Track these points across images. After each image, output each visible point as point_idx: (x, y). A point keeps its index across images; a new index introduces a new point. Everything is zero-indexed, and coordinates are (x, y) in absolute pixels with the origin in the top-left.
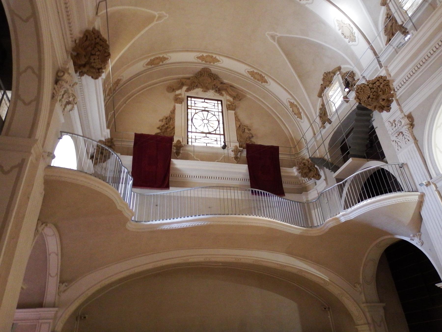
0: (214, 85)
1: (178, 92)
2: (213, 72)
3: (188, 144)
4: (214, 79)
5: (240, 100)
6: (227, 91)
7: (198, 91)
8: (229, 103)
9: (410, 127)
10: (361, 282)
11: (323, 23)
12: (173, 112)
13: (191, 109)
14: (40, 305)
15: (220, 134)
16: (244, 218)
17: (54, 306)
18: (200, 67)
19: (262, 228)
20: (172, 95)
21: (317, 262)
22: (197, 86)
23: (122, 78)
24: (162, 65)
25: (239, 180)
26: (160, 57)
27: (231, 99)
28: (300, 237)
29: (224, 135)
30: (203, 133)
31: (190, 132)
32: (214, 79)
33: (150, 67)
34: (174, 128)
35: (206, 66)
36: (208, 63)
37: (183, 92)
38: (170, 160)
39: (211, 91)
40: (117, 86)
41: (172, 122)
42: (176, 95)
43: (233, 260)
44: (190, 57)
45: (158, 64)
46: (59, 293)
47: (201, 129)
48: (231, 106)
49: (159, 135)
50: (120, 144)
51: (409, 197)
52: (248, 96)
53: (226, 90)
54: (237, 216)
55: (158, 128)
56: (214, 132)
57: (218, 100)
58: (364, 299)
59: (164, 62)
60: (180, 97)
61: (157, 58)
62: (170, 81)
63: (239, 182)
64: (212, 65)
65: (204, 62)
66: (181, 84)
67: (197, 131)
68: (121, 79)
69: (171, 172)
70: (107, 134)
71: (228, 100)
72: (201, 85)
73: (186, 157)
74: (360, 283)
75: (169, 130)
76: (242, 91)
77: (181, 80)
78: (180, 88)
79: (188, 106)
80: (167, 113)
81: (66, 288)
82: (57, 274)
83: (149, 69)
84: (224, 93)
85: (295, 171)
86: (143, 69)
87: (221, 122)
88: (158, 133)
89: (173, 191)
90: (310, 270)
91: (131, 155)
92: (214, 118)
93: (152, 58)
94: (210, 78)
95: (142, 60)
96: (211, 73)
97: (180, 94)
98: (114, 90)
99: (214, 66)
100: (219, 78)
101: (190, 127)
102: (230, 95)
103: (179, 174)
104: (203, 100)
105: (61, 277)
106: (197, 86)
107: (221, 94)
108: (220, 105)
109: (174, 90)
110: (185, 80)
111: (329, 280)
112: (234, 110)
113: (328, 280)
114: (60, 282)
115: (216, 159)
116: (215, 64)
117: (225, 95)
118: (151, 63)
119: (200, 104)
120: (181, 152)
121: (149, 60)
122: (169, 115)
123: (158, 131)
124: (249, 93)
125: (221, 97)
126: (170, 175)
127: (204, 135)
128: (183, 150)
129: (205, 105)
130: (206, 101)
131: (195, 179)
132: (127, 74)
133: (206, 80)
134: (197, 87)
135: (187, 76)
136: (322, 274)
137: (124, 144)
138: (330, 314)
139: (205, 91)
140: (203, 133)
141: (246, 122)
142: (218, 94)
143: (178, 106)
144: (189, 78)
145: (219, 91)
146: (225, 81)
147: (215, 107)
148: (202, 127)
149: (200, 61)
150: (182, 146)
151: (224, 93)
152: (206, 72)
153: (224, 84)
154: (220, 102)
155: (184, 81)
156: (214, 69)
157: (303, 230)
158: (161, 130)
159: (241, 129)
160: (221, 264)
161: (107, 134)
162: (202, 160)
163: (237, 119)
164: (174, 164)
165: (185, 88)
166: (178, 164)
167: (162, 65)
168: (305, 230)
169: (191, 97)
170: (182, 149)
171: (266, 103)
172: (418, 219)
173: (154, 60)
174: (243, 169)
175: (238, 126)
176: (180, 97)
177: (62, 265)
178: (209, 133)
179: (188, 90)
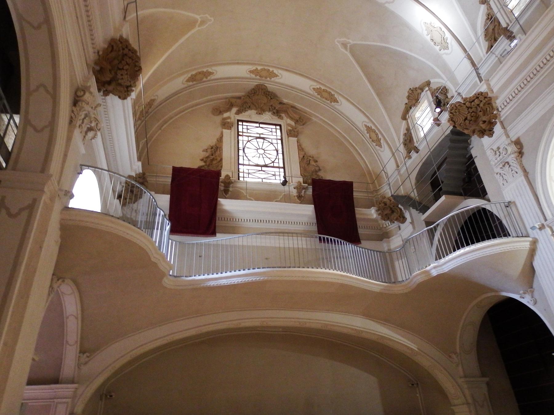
0: (272, 106)
1: (226, 115)
3: (239, 179)
4: (271, 99)
5: (304, 124)
6: (288, 114)
7: (251, 114)
8: (289, 128)
10: (458, 351)
11: (225, 211)
13: (242, 136)
14: (56, 381)
17: (73, 382)
18: (254, 83)
19: (332, 284)
20: (218, 119)
22: (250, 107)
23: (156, 98)
26: (203, 71)
27: (293, 123)
28: (380, 296)
29: (284, 168)
31: (241, 164)
32: (271, 99)
33: (191, 83)
34: (221, 160)
36: (264, 78)
37: (232, 115)
38: (217, 200)
40: (151, 107)
42: (224, 119)
43: (297, 325)
49: (203, 168)
51: (518, 244)
55: (202, 160)
56: (272, 165)
59: (209, 78)
60: (229, 120)
61: (200, 73)
64: (268, 81)
65: (258, 77)
66: (230, 105)
67: (251, 163)
69: (218, 214)
71: (289, 125)
72: (255, 106)
73: (237, 196)
76: (306, 113)
78: (229, 110)
80: (213, 142)
81: (87, 359)
84: (283, 115)
85: (373, 213)
86: (183, 86)
87: (280, 151)
88: (201, 167)
89: (220, 238)
91: (167, 194)
93: (194, 73)
94: (266, 97)
97: (229, 118)
99: (271, 82)
100: (277, 96)
102: (292, 119)
103: (229, 218)
104: (258, 125)
105: (81, 344)
107: (280, 117)
108: (278, 131)
109: (221, 113)
111: (418, 349)
113: (416, 350)
114: (80, 352)
117: (285, 118)
118: (192, 79)
119: (255, 130)
120: (231, 189)
121: (189, 75)
123: (202, 164)
126: (217, 219)
127: (260, 168)
129: (260, 131)
130: (261, 125)
132: (163, 92)
133: (261, 100)
134: (250, 108)
137: (160, 180)
139: (260, 114)
140: (257, 165)
141: (311, 151)
142: (277, 118)
143: (226, 131)
144: (239, 98)
145: (277, 113)
146: (285, 101)
147: (273, 134)
150: (232, 183)
151: (283, 115)
153: (284, 104)
155: (233, 101)
156: (271, 86)
158: (205, 162)
159: (306, 160)
160: (281, 330)
163: (300, 148)
164: (222, 205)
165: (234, 110)
168: (387, 286)
169: (242, 121)
172: (530, 272)
173: (196, 74)
174: (309, 210)
175: (302, 156)
178: (266, 166)
179: (238, 113)
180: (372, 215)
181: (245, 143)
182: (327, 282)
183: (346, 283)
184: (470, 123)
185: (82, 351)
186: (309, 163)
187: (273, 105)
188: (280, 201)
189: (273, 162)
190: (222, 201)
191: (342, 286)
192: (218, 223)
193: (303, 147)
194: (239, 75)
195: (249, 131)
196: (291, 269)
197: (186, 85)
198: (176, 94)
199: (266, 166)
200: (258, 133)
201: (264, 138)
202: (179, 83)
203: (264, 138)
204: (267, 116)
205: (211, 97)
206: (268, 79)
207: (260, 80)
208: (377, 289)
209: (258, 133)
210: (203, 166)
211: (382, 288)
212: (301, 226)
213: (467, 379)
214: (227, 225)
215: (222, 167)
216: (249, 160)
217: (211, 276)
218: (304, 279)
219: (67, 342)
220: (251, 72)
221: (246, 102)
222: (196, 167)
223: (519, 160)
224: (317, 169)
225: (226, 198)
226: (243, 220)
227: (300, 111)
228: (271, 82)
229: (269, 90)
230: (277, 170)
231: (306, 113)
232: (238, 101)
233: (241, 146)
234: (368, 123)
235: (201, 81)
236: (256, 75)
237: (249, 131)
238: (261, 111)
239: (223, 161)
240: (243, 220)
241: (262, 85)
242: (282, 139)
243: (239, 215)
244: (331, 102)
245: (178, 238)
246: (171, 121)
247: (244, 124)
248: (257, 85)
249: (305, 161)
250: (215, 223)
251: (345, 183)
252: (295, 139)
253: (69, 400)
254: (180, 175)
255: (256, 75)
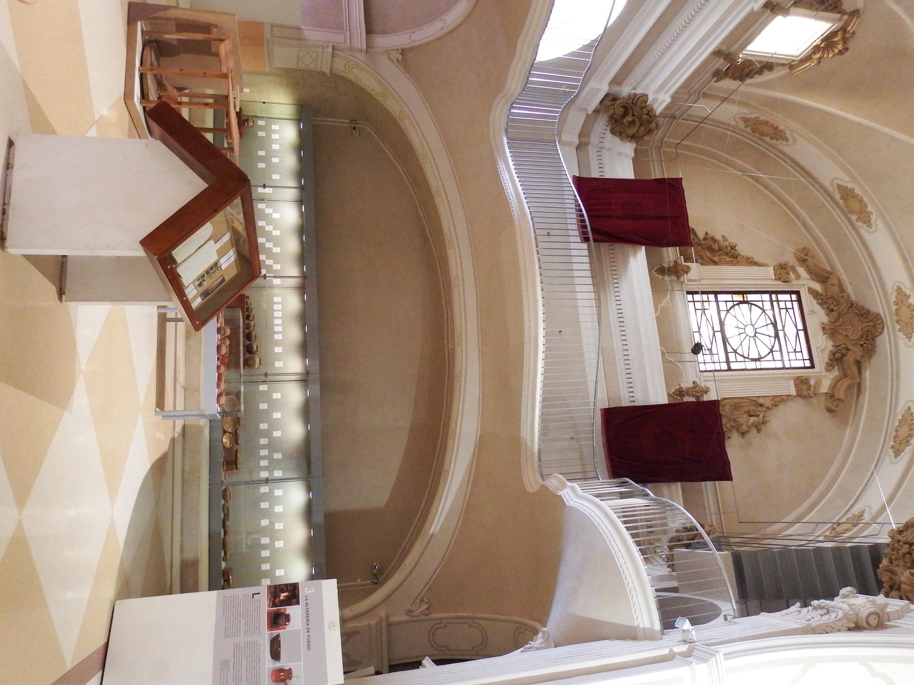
0: (848, 349)
1: (801, 271)
2: (879, 340)
3: (688, 293)
4: (862, 346)
5: (829, 410)
6: (842, 379)
7: (818, 316)
8: (812, 382)
9: (849, 620)
10: (433, 616)
11: (626, 262)
12: (751, 262)
13: (771, 301)
14: (369, 31)
15: (728, 362)
16: (536, 301)
17: (368, 46)
18: (878, 306)
19: (520, 328)
20: (791, 260)
21: (469, 509)
22: (832, 311)
23: (791, 142)
24: (851, 223)
25: (631, 394)
26: (866, 206)
27: (825, 387)
28: (515, 442)
29: (729, 369)
30: (722, 324)
31: (716, 297)
32: (862, 346)
33: (837, 196)
34: (715, 263)
35: (888, 319)
36: (895, 318)
37: (805, 282)
38: (641, 244)
39: (831, 343)
40: (772, 138)
41: (728, 259)
42: (793, 269)
43: (457, 331)
44: (894, 272)
45: (850, 212)
46: (387, 52)
47: (730, 322)
48: (805, 387)
49: (692, 236)
50: (655, 158)
51: (643, 604)
52: (848, 430)
53: (845, 375)
54: (538, 278)
55: (706, 234)
56: (729, 350)
57: (811, 359)
58: (395, 619)
59: (859, 224)
60: (792, 276)
61: (861, 201)
62: (821, 254)
63: (627, 395)
64: (893, 327)
65: (894, 307)
66: (822, 276)
67: (723, 314)
68: (787, 140)
69: (617, 246)
70: (663, 101)
71: (818, 383)
72: (837, 320)
74: (429, 614)
75: (708, 254)
76: (855, 415)
77: (831, 273)
79: (777, 293)
80: (743, 249)
81: (395, 60)
82: (414, 41)
83: (832, 198)
86: (826, 182)
87: (759, 365)
88: (695, 234)
89: (580, 251)
90: (449, 489)
92: (764, 351)
93: (857, 191)
94: (862, 336)
95: (847, 171)
96: (874, 338)
97: (798, 277)
98: (762, 134)
99: (894, 333)
100: (870, 357)
101: (728, 297)
102: (834, 386)
103: (618, 268)
104: (800, 326)
105: (411, 49)
106: (832, 311)
107: (830, 366)
108: (801, 364)
110: (836, 283)
111: (432, 535)
112: (799, 395)
113: (432, 531)
114: (403, 50)
115: (666, 348)
116: (900, 334)
118: (847, 194)
119: (791, 326)
120: (667, 278)
121: (850, 186)
122: (740, 252)
123: (701, 235)
124: (857, 429)
125: (823, 366)
126: (633, 404)
127: (717, 328)
128: (671, 281)
129: (791, 331)
130: (802, 334)
131: (596, 162)
132: (804, 149)
133: (853, 332)
135: (850, 289)
136: (444, 515)
137: (656, 165)
138: (364, 585)
139: (824, 328)
140: (722, 324)
141: (779, 420)
142: (827, 360)
143: (771, 271)
144: (842, 289)
145: (837, 359)
146: (867, 374)
148: (735, 323)
149: (893, 298)
150: (679, 278)
151: (836, 373)
152: (871, 324)
153: (860, 373)
154: (794, 297)
155: (833, 280)
156: (884, 341)
157: (532, 440)
158: (705, 239)
159: (757, 411)
160: (451, 347)
161: (663, 101)
162: (659, 320)
163: (779, 401)
164: (635, 254)
165: (817, 287)
166: (638, 261)
167: (851, 223)
168: (533, 453)
169: (799, 301)
170: (674, 278)
171: (844, 471)
172: (586, 632)
173: (856, 196)
175: (761, 401)
176: (792, 276)
177: (428, 44)
178: (725, 340)
179: (812, 291)
180: (674, 522)
181: (760, 304)
182: (522, 305)
183: (526, 350)
184: (904, 555)
185: (403, 52)
186: (751, 416)
187: (850, 353)
188: (665, 361)
189: (735, 352)
190: (642, 252)
191: (521, 346)
192: (604, 246)
193: (781, 406)
194: (885, 274)
195: (783, 311)
196: (536, 256)
197: (830, 189)
198: (807, 174)
199: (725, 340)
200: (784, 327)
201: (777, 336)
202: (830, 172)
203: (777, 336)
204: (823, 345)
205: (825, 242)
206: (898, 327)
207: (890, 312)
208: (525, 433)
209: (784, 327)
210: (697, 236)
211: (529, 444)
212: (626, 390)
213: (385, 627)
214: (605, 267)
215: (702, 264)
216: (728, 311)
217: (510, 159)
218: (522, 273)
219: (413, 32)
220: (899, 290)
221: (838, 304)
222: (692, 224)
223: (840, 624)
224: (744, 428)
225: (650, 271)
226: (617, 294)
227: (856, 408)
228: (894, 333)
229: (878, 340)
230: (723, 359)
231: (855, 415)
232: (837, 289)
233: (750, 297)
234: (870, 512)
235: (847, 211)
236: (896, 303)
237: (783, 311)
238: (831, 331)
239: (715, 267)
240: (617, 294)
241: (882, 323)
242: (784, 368)
243: (624, 287)
244: (892, 447)
245: (598, 419)
246: (762, 189)
247: (795, 304)
248: (878, 315)
249: (753, 408)
250: (603, 241)
251: (726, 464)
252: (793, 392)
253: (348, 44)
254: (670, 192)
255: (896, 303)
